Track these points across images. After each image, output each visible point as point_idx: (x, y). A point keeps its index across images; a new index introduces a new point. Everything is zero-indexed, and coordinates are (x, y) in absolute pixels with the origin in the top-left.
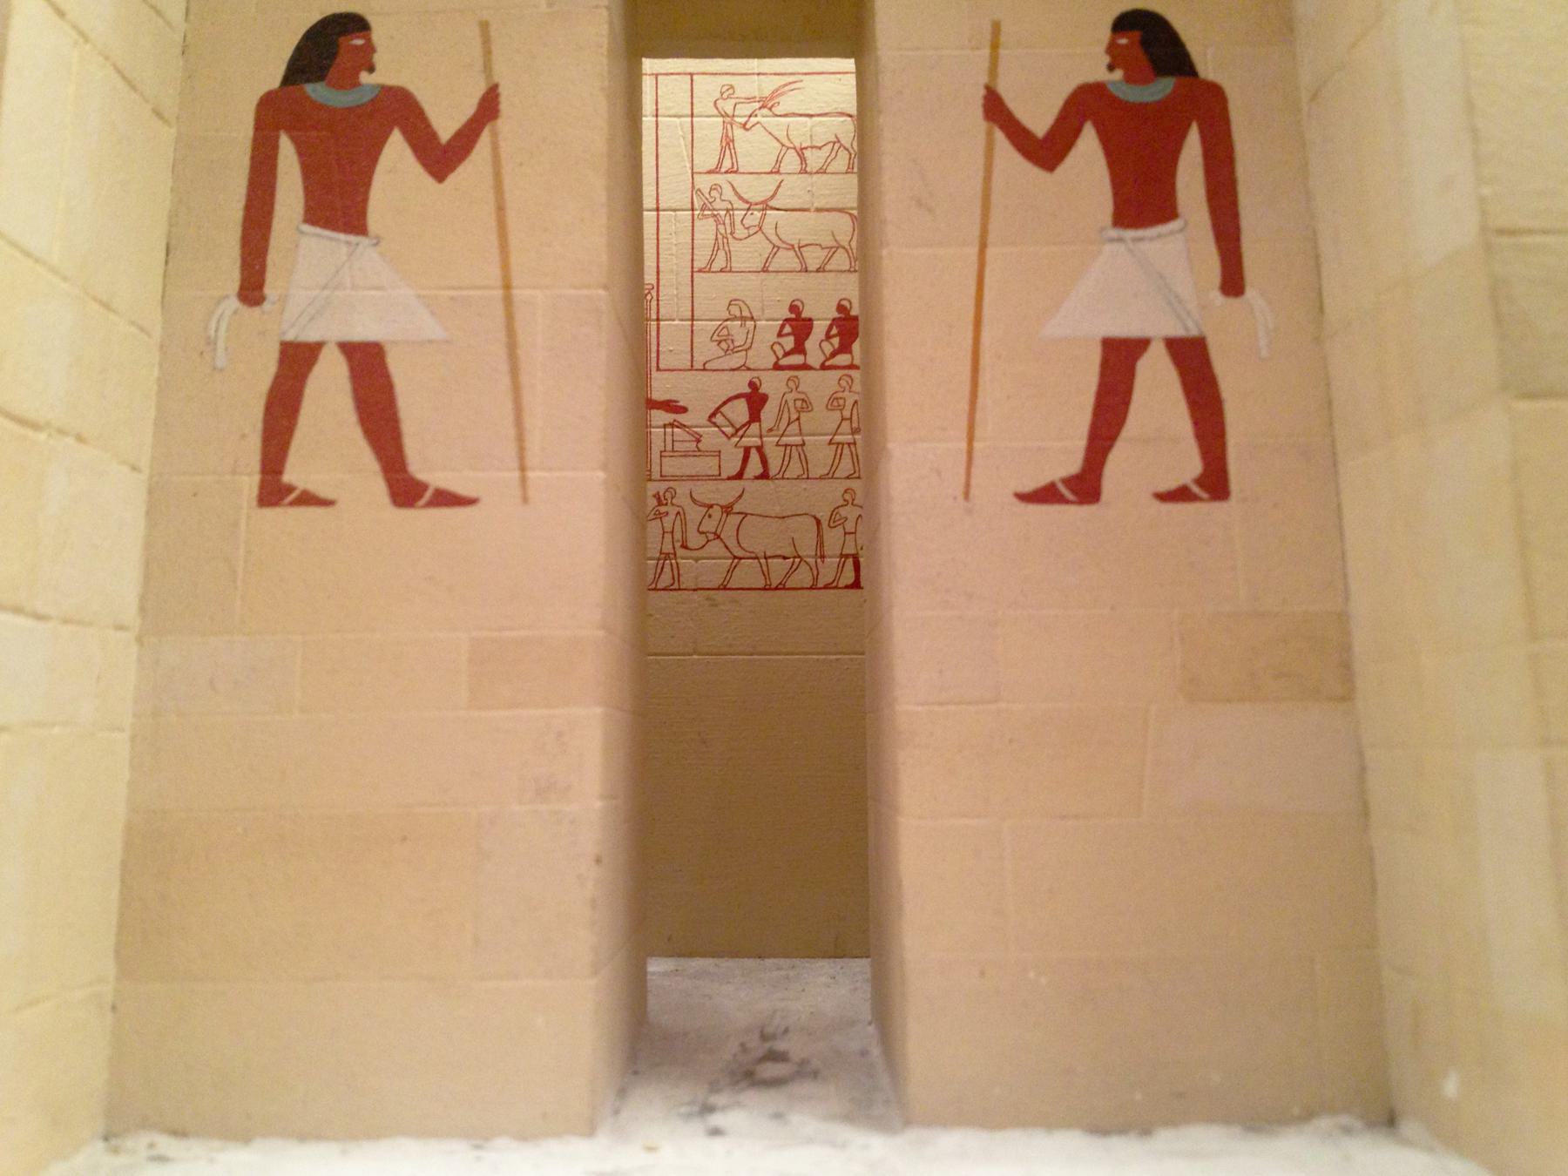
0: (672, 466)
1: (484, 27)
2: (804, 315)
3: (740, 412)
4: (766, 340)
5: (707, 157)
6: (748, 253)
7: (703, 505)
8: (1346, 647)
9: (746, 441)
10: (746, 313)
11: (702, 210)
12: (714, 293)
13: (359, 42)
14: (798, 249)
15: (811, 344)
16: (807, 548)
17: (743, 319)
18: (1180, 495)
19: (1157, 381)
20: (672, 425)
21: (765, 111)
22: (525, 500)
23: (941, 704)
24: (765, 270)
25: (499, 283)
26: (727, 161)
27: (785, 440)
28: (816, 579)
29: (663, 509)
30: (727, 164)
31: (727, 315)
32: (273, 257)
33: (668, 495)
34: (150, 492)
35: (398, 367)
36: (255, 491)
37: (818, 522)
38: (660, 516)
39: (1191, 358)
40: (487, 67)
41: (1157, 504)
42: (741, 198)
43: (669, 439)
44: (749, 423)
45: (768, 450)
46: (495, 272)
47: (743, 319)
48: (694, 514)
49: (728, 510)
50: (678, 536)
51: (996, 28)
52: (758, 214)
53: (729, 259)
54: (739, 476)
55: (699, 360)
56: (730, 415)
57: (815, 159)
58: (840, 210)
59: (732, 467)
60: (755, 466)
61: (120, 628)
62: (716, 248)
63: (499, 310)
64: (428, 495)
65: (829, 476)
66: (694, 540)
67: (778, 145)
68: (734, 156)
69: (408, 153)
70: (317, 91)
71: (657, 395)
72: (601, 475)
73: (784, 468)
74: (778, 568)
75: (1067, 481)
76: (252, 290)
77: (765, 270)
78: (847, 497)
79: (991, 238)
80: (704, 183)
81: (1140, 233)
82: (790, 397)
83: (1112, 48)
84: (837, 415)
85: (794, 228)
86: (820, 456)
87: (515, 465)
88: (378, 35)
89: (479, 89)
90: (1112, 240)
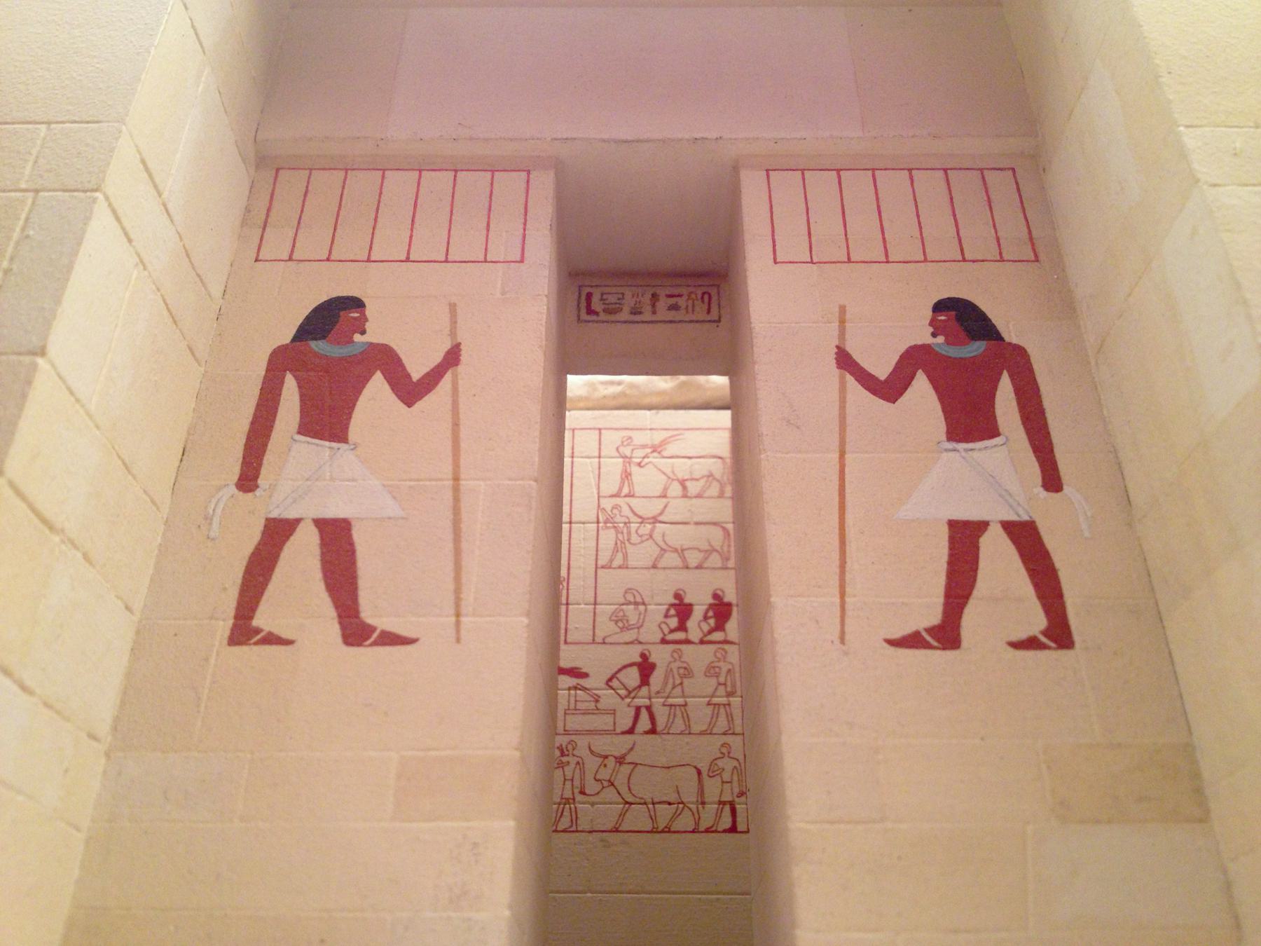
0: (574, 722)
1: (453, 308)
2: (687, 601)
3: (632, 677)
4: (655, 620)
5: (611, 484)
6: (641, 554)
7: (601, 756)
8: (1196, 775)
9: (639, 702)
10: (639, 599)
11: (605, 523)
12: (613, 585)
13: (356, 315)
14: (680, 552)
15: (691, 624)
16: (690, 796)
17: (636, 604)
18: (1031, 644)
19: (997, 554)
20: (575, 688)
21: (655, 454)
22: (458, 640)
23: (832, 822)
24: (654, 567)
25: (450, 476)
26: (626, 489)
27: (671, 701)
28: (697, 824)
29: (565, 759)
30: (625, 491)
31: (622, 601)
32: (269, 458)
33: (570, 747)
34: (138, 632)
35: (359, 536)
36: (227, 633)
37: (699, 772)
38: (561, 765)
39: (1025, 537)
40: (453, 333)
41: (1010, 649)
42: (635, 514)
43: (572, 699)
44: (640, 687)
45: (654, 709)
46: (447, 470)
47: (636, 604)
48: (592, 764)
49: (620, 760)
50: (577, 783)
51: (843, 310)
52: (649, 526)
53: (625, 556)
54: (631, 731)
55: (600, 634)
56: (623, 680)
57: (693, 488)
58: (715, 524)
59: (626, 723)
60: (644, 723)
61: (92, 737)
62: (616, 550)
63: (449, 495)
64: (375, 635)
65: (707, 733)
66: (592, 787)
67: (664, 478)
68: (631, 485)
69: (387, 387)
70: (318, 346)
71: (564, 664)
72: (525, 620)
73: (669, 725)
74: (664, 813)
75: (930, 630)
76: (248, 481)
77: (654, 567)
78: (724, 750)
79: (848, 448)
80: (607, 504)
81: (971, 445)
82: (674, 666)
83: (932, 323)
84: (713, 681)
85: (677, 536)
86: (700, 716)
87: (452, 611)
88: (369, 312)
89: (447, 345)
90: (946, 450)
